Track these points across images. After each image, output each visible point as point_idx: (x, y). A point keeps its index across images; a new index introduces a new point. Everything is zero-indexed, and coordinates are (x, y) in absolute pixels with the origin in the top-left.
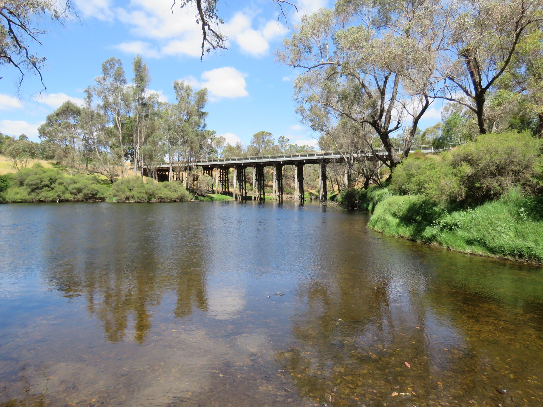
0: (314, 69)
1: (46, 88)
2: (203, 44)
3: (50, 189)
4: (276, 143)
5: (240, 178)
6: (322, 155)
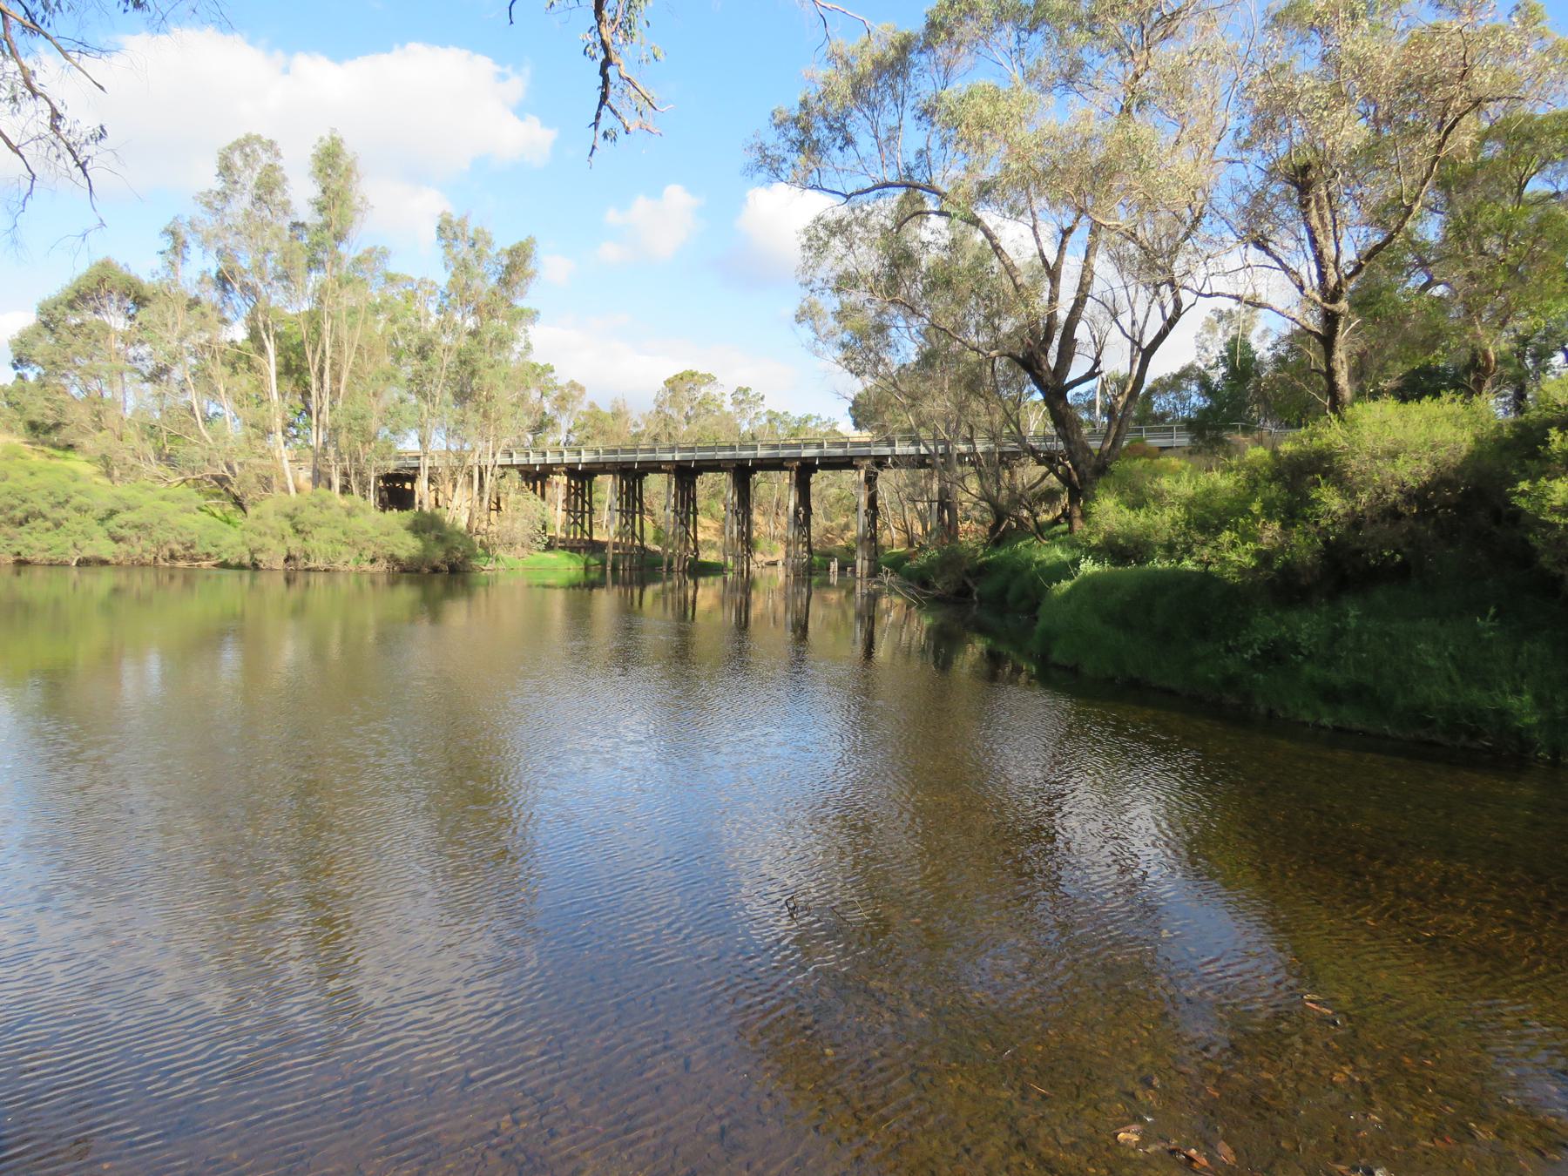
0: (860, 197)
1: (103, 224)
2: (598, 116)
3: (49, 524)
4: (728, 407)
5: (628, 504)
6: (867, 444)
